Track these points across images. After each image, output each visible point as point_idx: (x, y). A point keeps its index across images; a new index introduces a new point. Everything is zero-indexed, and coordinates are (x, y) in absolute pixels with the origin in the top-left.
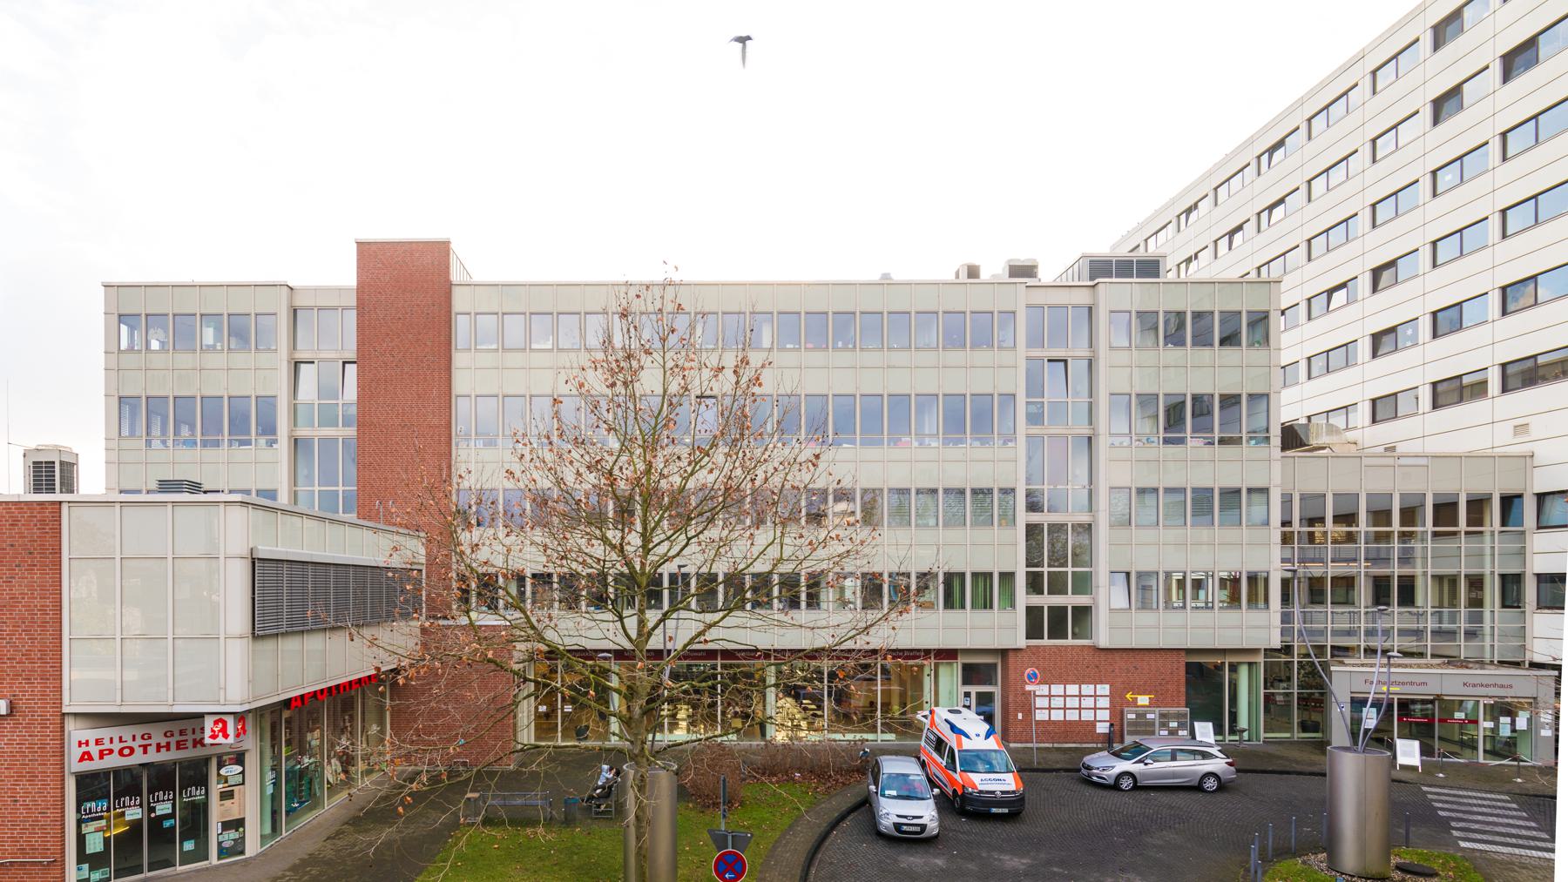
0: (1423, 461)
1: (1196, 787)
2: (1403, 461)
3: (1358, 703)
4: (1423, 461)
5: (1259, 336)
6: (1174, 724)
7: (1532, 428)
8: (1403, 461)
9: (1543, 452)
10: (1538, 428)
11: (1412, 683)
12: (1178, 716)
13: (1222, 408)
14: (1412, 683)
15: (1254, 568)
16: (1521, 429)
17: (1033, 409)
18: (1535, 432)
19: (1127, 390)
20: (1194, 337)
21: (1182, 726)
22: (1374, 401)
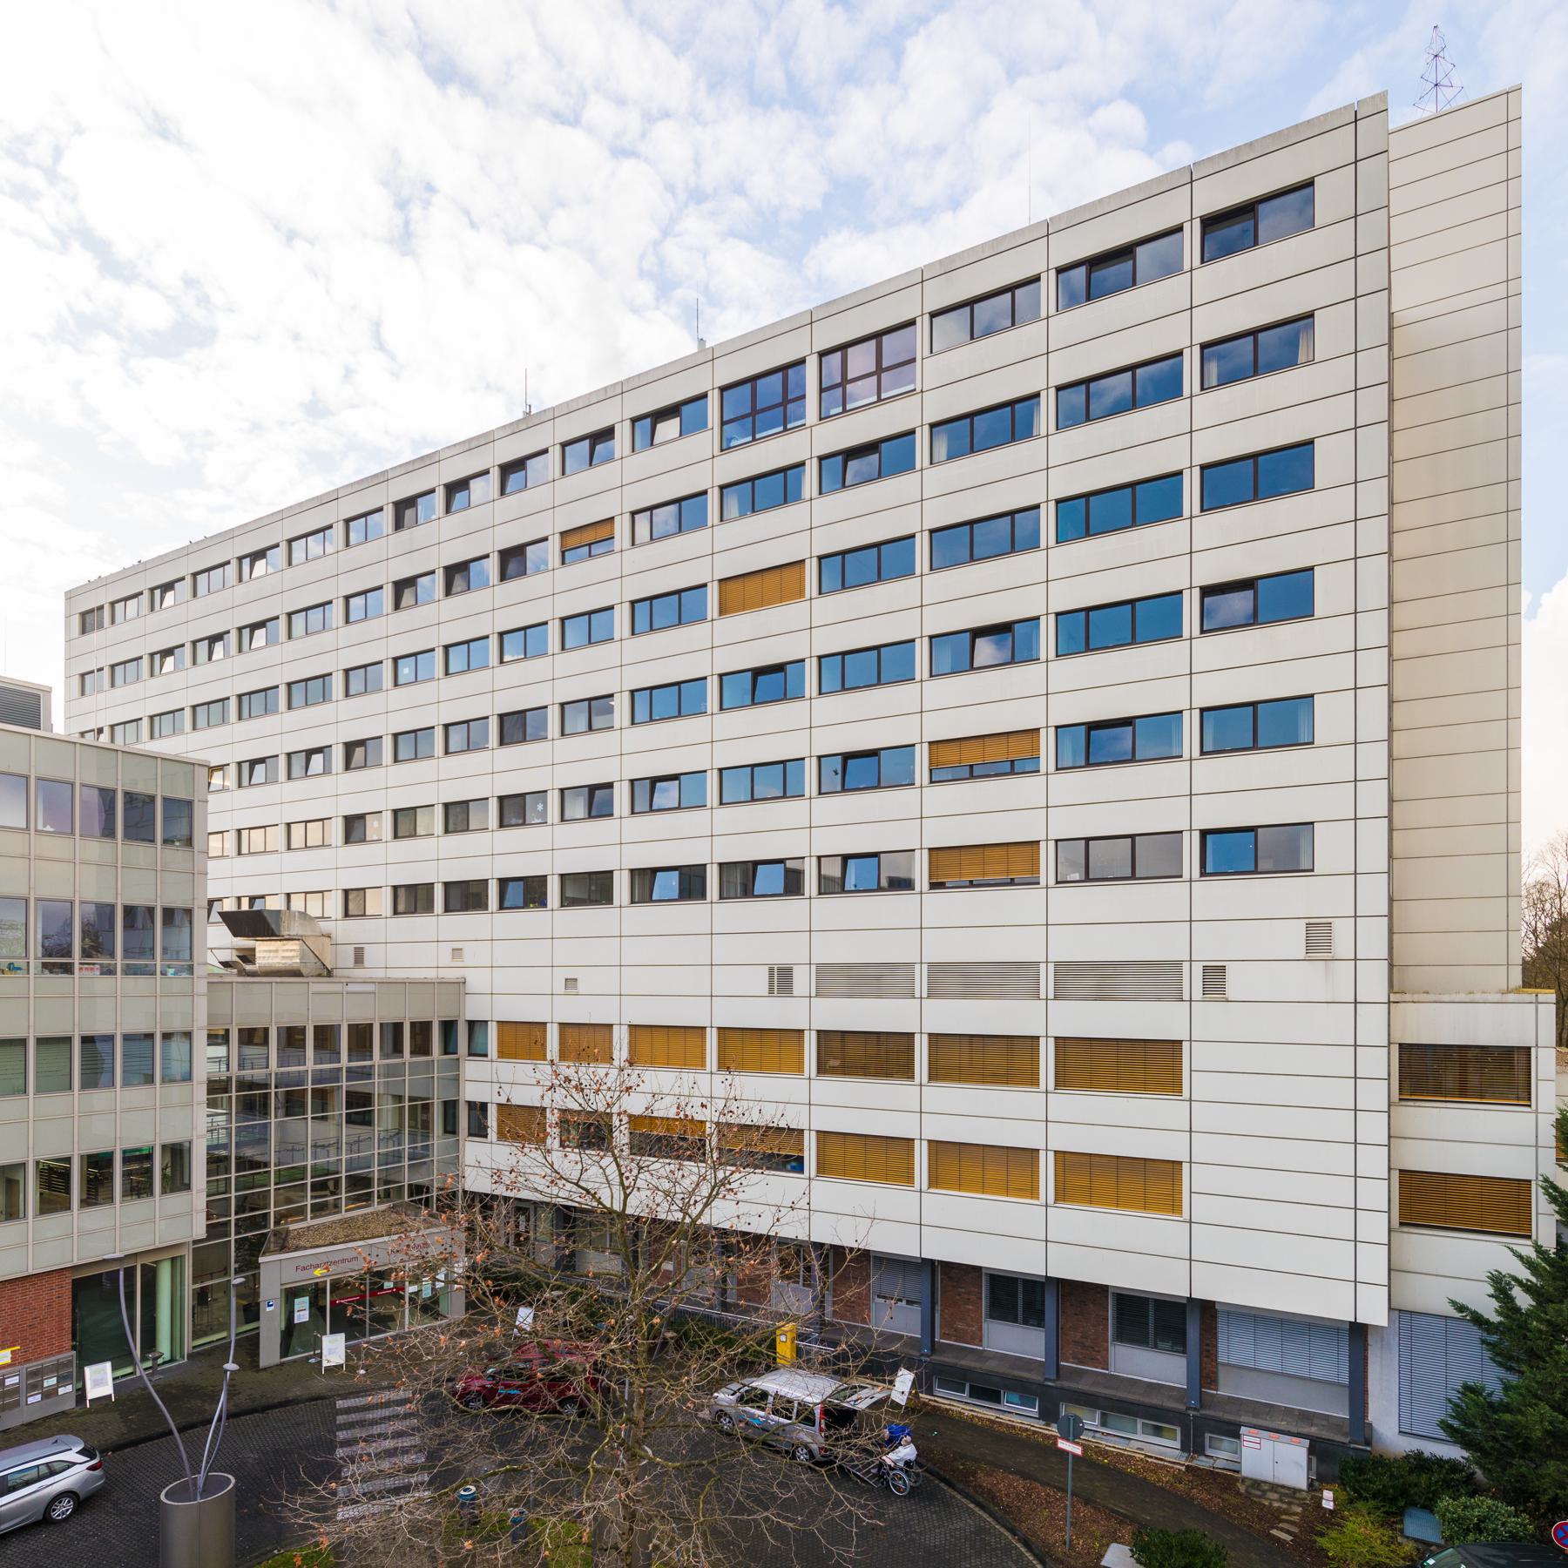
0: (370, 988)
1: (42, 1521)
2: (351, 988)
3: (291, 1294)
4: (370, 988)
5: (180, 830)
6: (50, 1382)
7: (466, 953)
8: (351, 988)
9: (477, 980)
10: (472, 954)
11: (343, 1261)
12: (57, 1367)
13: (70, 945)
14: (343, 1261)
15: (172, 1138)
16: (457, 952)
17: (578, 808)
18: (468, 959)
19: (21, 890)
20: (126, 826)
21: (62, 1380)
22: (346, 892)
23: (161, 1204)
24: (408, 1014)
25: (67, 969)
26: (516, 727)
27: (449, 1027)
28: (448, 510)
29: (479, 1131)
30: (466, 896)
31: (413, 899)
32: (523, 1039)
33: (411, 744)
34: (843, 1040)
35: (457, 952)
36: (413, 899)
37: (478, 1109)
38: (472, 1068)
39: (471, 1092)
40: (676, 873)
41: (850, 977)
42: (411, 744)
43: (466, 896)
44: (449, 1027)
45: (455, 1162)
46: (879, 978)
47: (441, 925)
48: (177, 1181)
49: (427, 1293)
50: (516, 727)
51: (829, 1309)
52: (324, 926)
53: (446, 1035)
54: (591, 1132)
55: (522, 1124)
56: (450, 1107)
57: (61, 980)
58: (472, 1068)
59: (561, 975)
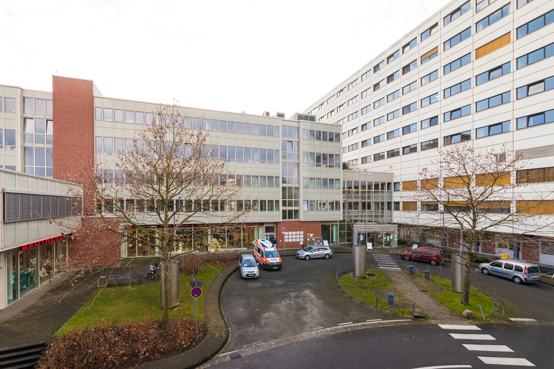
3: (359, 234)
9: (396, 173)
16: (391, 167)
18: (394, 168)
21: (320, 242)
23: (335, 212)
24: (380, 180)
25: (320, 166)
26: (406, 109)
27: (389, 184)
28: (388, 63)
29: (397, 209)
30: (393, 154)
31: (378, 157)
32: (410, 186)
33: (377, 121)
34: (528, 174)
35: (391, 167)
36: (378, 157)
37: (397, 203)
38: (395, 194)
39: (395, 199)
40: (460, 135)
41: (531, 152)
42: (377, 121)
43: (393, 154)
44: (389, 184)
45: (391, 216)
46: (545, 150)
47: (387, 161)
48: (338, 208)
49: (388, 240)
50: (406, 109)
51: (524, 180)
52: (357, 166)
53: (389, 186)
54: (431, 207)
55: (409, 206)
56: (389, 203)
57: (318, 168)
58: (395, 194)
59: (421, 168)
